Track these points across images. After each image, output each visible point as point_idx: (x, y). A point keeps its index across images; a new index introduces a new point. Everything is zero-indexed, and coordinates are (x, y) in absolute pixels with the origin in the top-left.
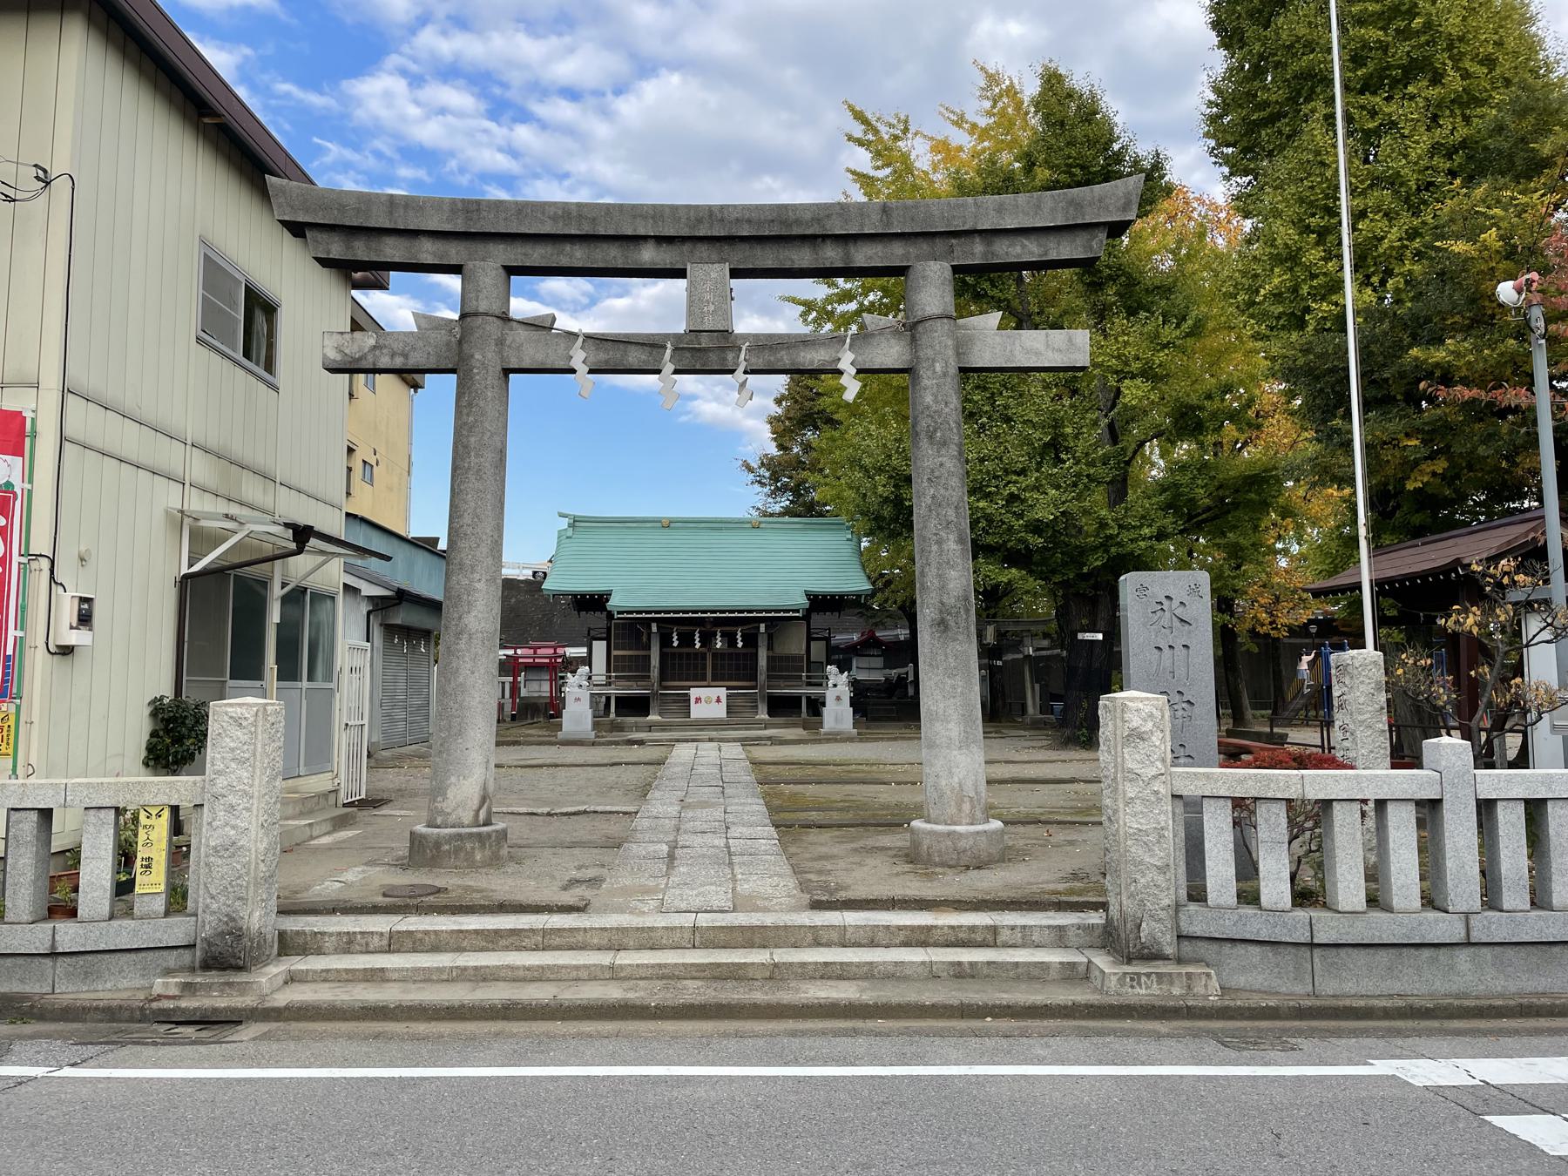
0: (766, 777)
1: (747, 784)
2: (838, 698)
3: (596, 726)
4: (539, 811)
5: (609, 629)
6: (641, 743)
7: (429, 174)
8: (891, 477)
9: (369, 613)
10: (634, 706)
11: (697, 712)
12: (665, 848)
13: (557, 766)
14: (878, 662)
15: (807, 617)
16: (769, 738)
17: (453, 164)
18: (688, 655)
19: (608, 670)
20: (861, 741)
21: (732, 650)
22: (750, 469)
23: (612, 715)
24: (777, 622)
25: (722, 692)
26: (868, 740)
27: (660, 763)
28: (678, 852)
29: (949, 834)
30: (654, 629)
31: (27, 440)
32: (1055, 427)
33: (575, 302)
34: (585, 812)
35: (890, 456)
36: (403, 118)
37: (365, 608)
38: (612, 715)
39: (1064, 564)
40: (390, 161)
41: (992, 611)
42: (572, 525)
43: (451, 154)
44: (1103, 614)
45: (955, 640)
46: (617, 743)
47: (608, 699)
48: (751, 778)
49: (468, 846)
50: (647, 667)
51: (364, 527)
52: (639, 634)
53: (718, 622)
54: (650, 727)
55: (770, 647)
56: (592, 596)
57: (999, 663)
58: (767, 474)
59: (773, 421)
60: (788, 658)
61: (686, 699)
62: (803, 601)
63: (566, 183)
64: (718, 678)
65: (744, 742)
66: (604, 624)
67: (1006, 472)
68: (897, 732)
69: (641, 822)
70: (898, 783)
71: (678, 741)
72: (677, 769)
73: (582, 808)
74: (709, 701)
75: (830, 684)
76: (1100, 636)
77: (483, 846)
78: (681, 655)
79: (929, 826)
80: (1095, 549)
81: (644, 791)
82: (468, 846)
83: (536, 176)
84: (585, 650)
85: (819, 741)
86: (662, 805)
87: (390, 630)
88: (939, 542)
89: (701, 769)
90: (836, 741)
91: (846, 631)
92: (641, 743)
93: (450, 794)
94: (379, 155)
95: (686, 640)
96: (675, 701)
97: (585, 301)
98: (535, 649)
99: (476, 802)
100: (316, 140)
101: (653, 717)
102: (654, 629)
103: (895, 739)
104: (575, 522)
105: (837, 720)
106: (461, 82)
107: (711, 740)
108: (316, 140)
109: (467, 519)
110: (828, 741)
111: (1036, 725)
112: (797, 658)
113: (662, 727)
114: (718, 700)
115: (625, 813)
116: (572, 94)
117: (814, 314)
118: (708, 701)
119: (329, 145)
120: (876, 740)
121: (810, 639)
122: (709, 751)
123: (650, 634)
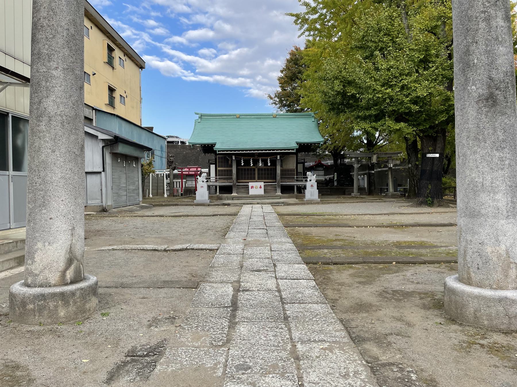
0: (289, 224)
1: (279, 227)
2: (312, 186)
3: (210, 198)
4: (160, 248)
5: (216, 159)
6: (229, 205)
7: (161, 14)
8: (341, 82)
9: (103, 147)
10: (226, 190)
11: (252, 192)
12: (230, 290)
13: (188, 216)
14: (322, 173)
15: (296, 154)
16: (283, 203)
17: (169, 11)
18: (248, 169)
19: (216, 175)
20: (322, 203)
21: (265, 167)
22: (271, 98)
23: (218, 194)
24: (285, 154)
25: (262, 184)
26: (325, 203)
27: (235, 214)
28: (242, 296)
29: (500, 300)
30: (234, 158)
31: (190, 173)
32: (426, 51)
33: (210, 57)
34: (186, 249)
35: (341, 72)
37: (101, 145)
38: (218, 194)
39: (425, 120)
40: (148, 10)
41: (372, 151)
42: (201, 117)
43: (168, 7)
44: (439, 145)
45: (504, 114)
46: (218, 205)
47: (216, 187)
48: (279, 224)
49: (51, 304)
50: (231, 174)
51: (118, 119)
52: (228, 160)
53: (260, 155)
54: (233, 198)
55: (281, 166)
56: (208, 145)
57: (373, 172)
58: (278, 100)
59: (280, 79)
60: (288, 170)
61: (247, 187)
62: (296, 146)
63: (207, 15)
64: (260, 179)
65: (272, 204)
66: (214, 158)
67: (401, 75)
68: (337, 200)
69: (219, 259)
70: (358, 227)
71: (244, 204)
72: (243, 218)
73: (184, 246)
74: (256, 188)
75: (308, 180)
76: (437, 155)
77: (66, 303)
78: (245, 169)
79: (476, 291)
80: (442, 112)
81: (224, 233)
82: (51, 304)
83: (197, 13)
84: (207, 170)
85: (304, 204)
86: (233, 245)
87: (115, 156)
88: (488, 20)
89: (255, 219)
90: (311, 204)
91: (310, 162)
92: (229, 205)
93: (37, 258)
94: (144, 8)
95: (247, 163)
97: (214, 56)
98: (189, 168)
99: (62, 265)
100: (124, 4)
101: (234, 194)
102: (234, 158)
103: (337, 203)
104: (201, 117)
105: (311, 195)
107: (258, 204)
108: (124, 4)
109: (43, 13)
110: (308, 204)
111: (393, 196)
112: (292, 170)
113: (238, 198)
114: (261, 187)
115: (211, 250)
117: (300, 20)
118: (256, 188)
119: (128, 5)
120: (328, 203)
121: (297, 163)
122: (257, 208)
123: (232, 160)
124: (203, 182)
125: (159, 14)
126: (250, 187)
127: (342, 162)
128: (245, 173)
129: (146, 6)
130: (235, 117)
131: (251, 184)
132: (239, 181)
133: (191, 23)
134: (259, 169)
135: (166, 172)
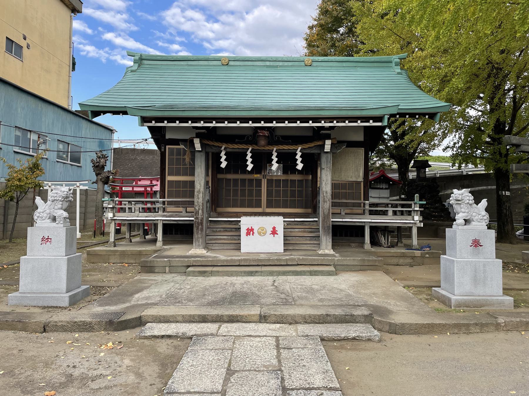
2: (476, 243)
11: (250, 245)
17: (193, 36)
23: (159, 244)
25: (278, 222)
30: (198, 146)
36: (179, 23)
43: (193, 33)
47: (156, 225)
74: (262, 233)
94: (171, 34)
95: (237, 161)
96: (226, 230)
102: (198, 146)
105: (475, 281)
106: (198, 10)
114: (274, 232)
116: (232, 13)
118: (262, 232)
119: (154, 31)
123: (193, 152)
124: (54, 219)
125: (183, 39)
126: (243, 232)
127: (422, 175)
128: (243, 191)
129: (173, 32)
130: (219, 63)
131: (246, 222)
132: (220, 210)
133: (213, 48)
134: (270, 182)
135: (82, 187)
